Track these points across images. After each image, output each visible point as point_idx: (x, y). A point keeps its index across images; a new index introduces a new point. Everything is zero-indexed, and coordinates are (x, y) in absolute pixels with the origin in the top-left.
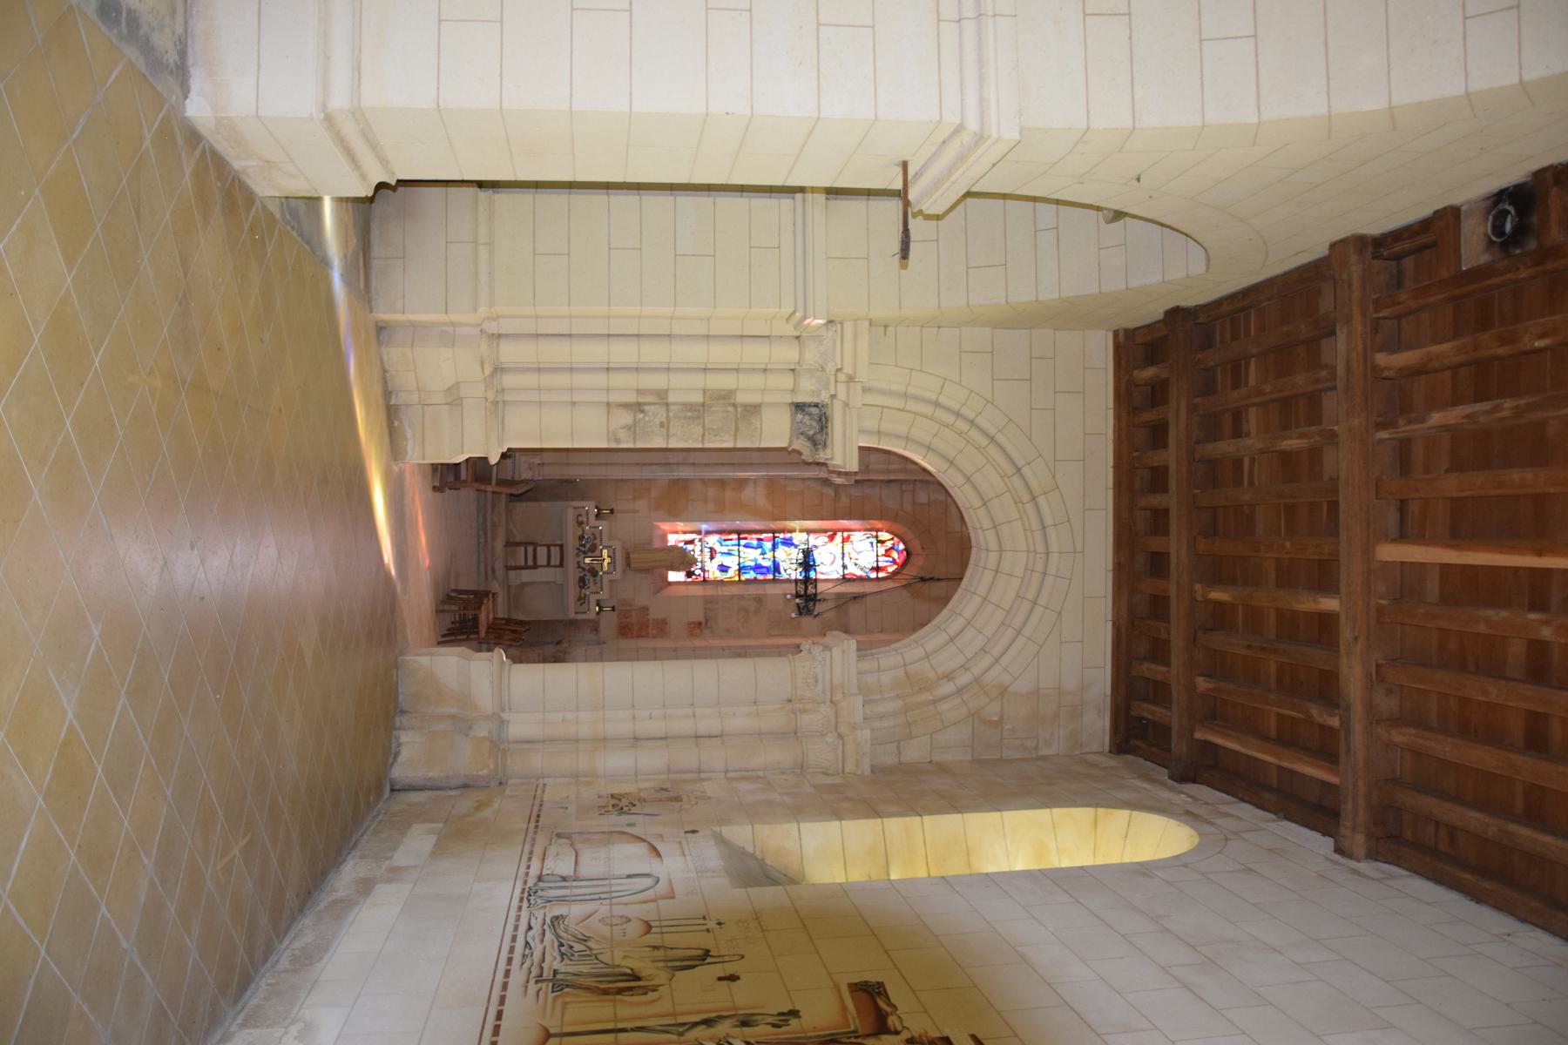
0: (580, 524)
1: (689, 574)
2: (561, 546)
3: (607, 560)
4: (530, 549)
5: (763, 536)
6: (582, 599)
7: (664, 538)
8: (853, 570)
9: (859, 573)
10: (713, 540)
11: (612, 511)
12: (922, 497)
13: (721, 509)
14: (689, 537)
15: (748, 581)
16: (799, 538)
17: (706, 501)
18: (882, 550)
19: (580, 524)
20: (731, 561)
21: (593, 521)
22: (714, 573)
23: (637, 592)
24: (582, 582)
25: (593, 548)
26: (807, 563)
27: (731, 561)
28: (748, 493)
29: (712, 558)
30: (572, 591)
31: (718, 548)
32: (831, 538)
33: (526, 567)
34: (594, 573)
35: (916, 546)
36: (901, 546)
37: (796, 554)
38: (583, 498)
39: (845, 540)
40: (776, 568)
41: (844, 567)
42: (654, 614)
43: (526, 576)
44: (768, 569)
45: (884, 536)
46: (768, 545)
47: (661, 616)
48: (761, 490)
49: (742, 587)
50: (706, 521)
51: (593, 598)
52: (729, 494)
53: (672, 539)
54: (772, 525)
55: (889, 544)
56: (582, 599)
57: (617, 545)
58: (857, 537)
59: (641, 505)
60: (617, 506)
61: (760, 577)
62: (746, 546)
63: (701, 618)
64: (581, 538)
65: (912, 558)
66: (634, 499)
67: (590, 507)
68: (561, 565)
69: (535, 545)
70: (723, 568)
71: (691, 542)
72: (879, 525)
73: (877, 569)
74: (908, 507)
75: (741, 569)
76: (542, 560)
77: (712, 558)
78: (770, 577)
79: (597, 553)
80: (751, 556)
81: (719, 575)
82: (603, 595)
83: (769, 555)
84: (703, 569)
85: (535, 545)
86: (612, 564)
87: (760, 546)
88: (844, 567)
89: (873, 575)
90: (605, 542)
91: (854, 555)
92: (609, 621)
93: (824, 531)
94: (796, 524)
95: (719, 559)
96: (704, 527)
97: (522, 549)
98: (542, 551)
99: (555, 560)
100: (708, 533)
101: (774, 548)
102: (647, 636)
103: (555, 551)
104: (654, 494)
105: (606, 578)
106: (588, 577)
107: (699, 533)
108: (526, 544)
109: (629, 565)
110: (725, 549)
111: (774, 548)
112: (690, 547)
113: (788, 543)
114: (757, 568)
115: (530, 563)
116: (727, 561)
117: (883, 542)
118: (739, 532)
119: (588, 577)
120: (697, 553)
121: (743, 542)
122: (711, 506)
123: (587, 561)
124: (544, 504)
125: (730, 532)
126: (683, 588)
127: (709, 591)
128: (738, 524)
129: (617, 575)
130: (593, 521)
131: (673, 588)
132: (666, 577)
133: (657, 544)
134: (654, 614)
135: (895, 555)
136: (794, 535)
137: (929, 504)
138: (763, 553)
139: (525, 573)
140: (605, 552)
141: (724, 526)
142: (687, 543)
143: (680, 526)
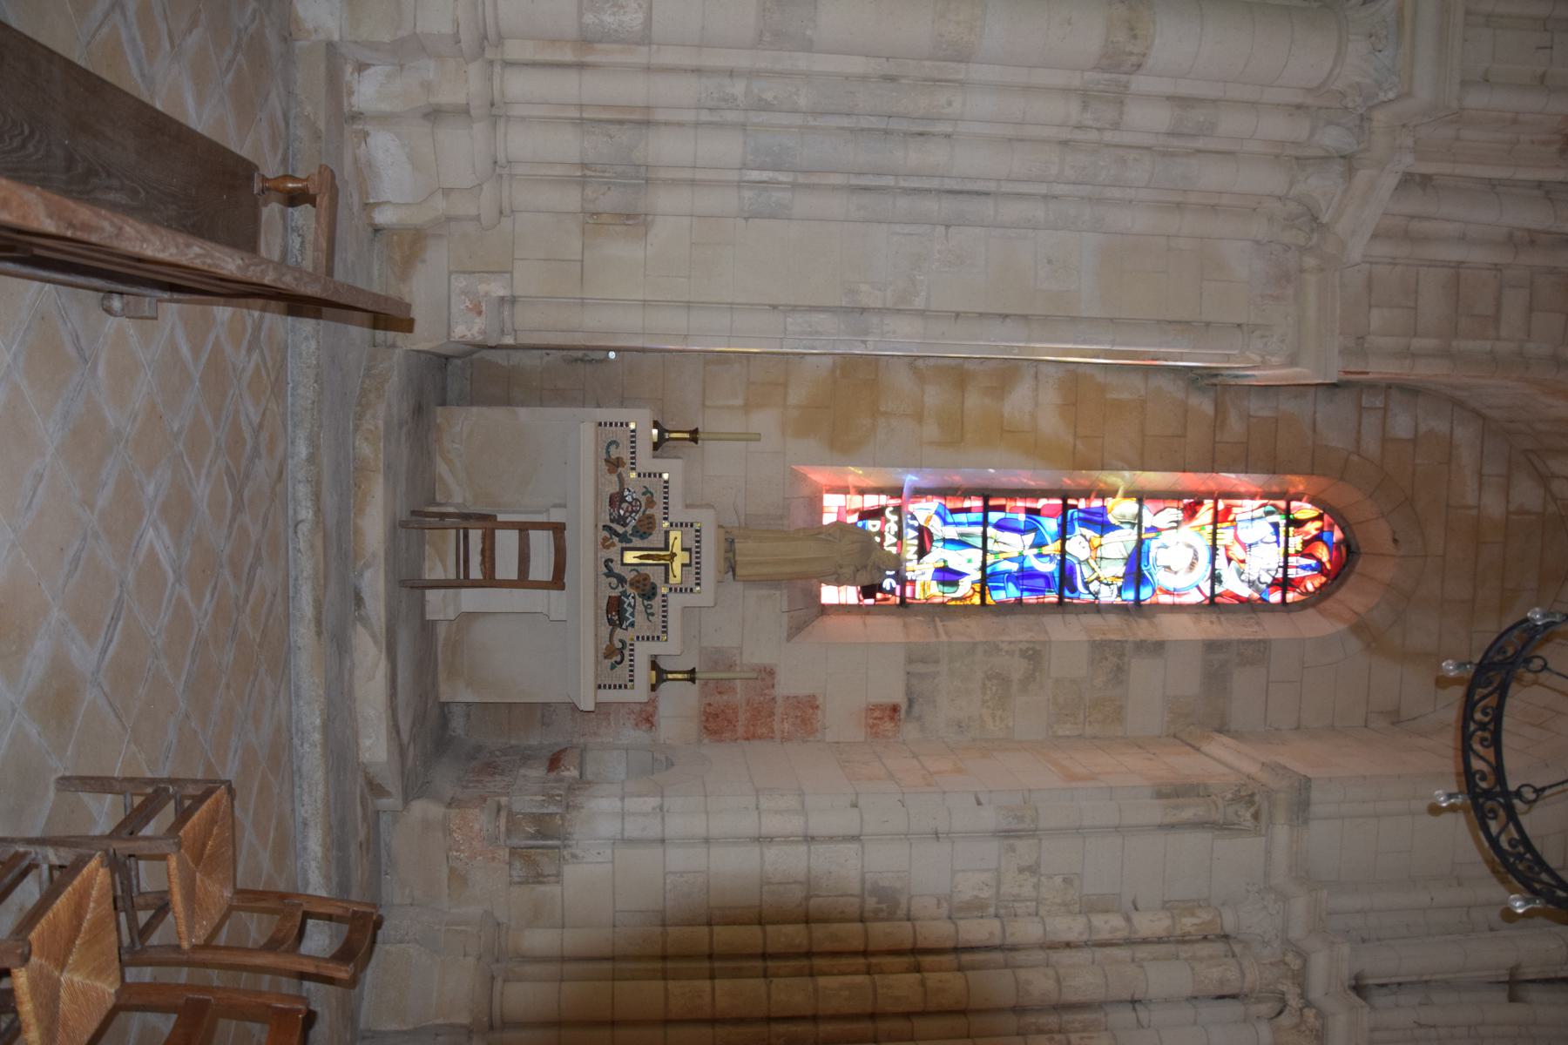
0: (614, 465)
1: (868, 591)
2: (558, 529)
3: (681, 558)
4: (475, 536)
5: (1041, 503)
6: (616, 654)
7: (817, 508)
8: (1232, 584)
9: (1245, 592)
10: (924, 511)
11: (694, 436)
12: (1402, 425)
13: (955, 434)
14: (871, 501)
15: (1001, 605)
16: (1120, 508)
17: (919, 417)
18: (1296, 543)
19: (614, 465)
20: (967, 562)
21: (646, 460)
22: (925, 587)
23: (746, 629)
24: (616, 611)
25: (646, 528)
26: (1136, 573)
27: (967, 562)
28: (1018, 402)
29: (922, 552)
30: (588, 629)
31: (936, 527)
32: (1191, 512)
33: (463, 582)
34: (649, 592)
35: (1377, 533)
36: (1338, 535)
37: (1119, 544)
38: (623, 402)
39: (1218, 518)
40: (1066, 574)
41: (1215, 578)
42: (789, 685)
43: (470, 599)
44: (1046, 577)
45: (1304, 510)
46: (1051, 525)
47: (802, 690)
48: (1050, 397)
49: (989, 621)
50: (907, 465)
51: (643, 652)
52: (974, 401)
53: (833, 507)
54: (1067, 481)
55: (1312, 528)
56: (616, 654)
57: (706, 520)
58: (1246, 509)
59: (764, 421)
60: (707, 424)
61: (1029, 598)
62: (1000, 526)
63: (899, 698)
64: (616, 500)
65: (1361, 565)
66: (747, 408)
67: (640, 422)
68: (558, 582)
69: (489, 524)
70: (947, 576)
71: (877, 513)
72: (1299, 483)
73: (1284, 584)
74: (1371, 445)
75: (988, 579)
76: (507, 567)
77: (922, 552)
78: (1052, 597)
79: (656, 539)
80: (1011, 548)
81: (935, 591)
82: (671, 649)
83: (1053, 548)
84: (902, 581)
85: (489, 524)
86: (693, 565)
87: (1031, 528)
88: (1215, 578)
89: (1275, 597)
90: (677, 513)
91: (1237, 552)
92: (679, 702)
93: (1172, 496)
94: (1120, 479)
95: (938, 555)
96: (910, 479)
97: (453, 532)
98: (507, 542)
99: (541, 568)
100: (919, 493)
101: (1063, 533)
102: (770, 736)
103: (541, 542)
104: (797, 395)
105: (675, 601)
106: (633, 599)
107: (896, 492)
108: (468, 518)
109: (733, 568)
110: (951, 532)
111: (1063, 533)
112: (873, 525)
113: (1099, 523)
114: (1025, 576)
115: (476, 573)
116: (958, 559)
117: (1299, 524)
118: (986, 495)
119: (633, 599)
120: (890, 539)
121: (994, 517)
122: (931, 430)
123: (630, 557)
124: (523, 413)
125: (967, 493)
126: (854, 621)
127: (919, 631)
128: (993, 475)
129: (705, 595)
130: (646, 460)
131: (831, 621)
132: (818, 596)
133: (1387, 812)
134: (789, 685)
135: (1323, 553)
136: (1109, 502)
137: (1415, 441)
138: (1039, 544)
139: (466, 593)
140: (675, 535)
141: (957, 478)
142: (866, 515)
143: (856, 474)
